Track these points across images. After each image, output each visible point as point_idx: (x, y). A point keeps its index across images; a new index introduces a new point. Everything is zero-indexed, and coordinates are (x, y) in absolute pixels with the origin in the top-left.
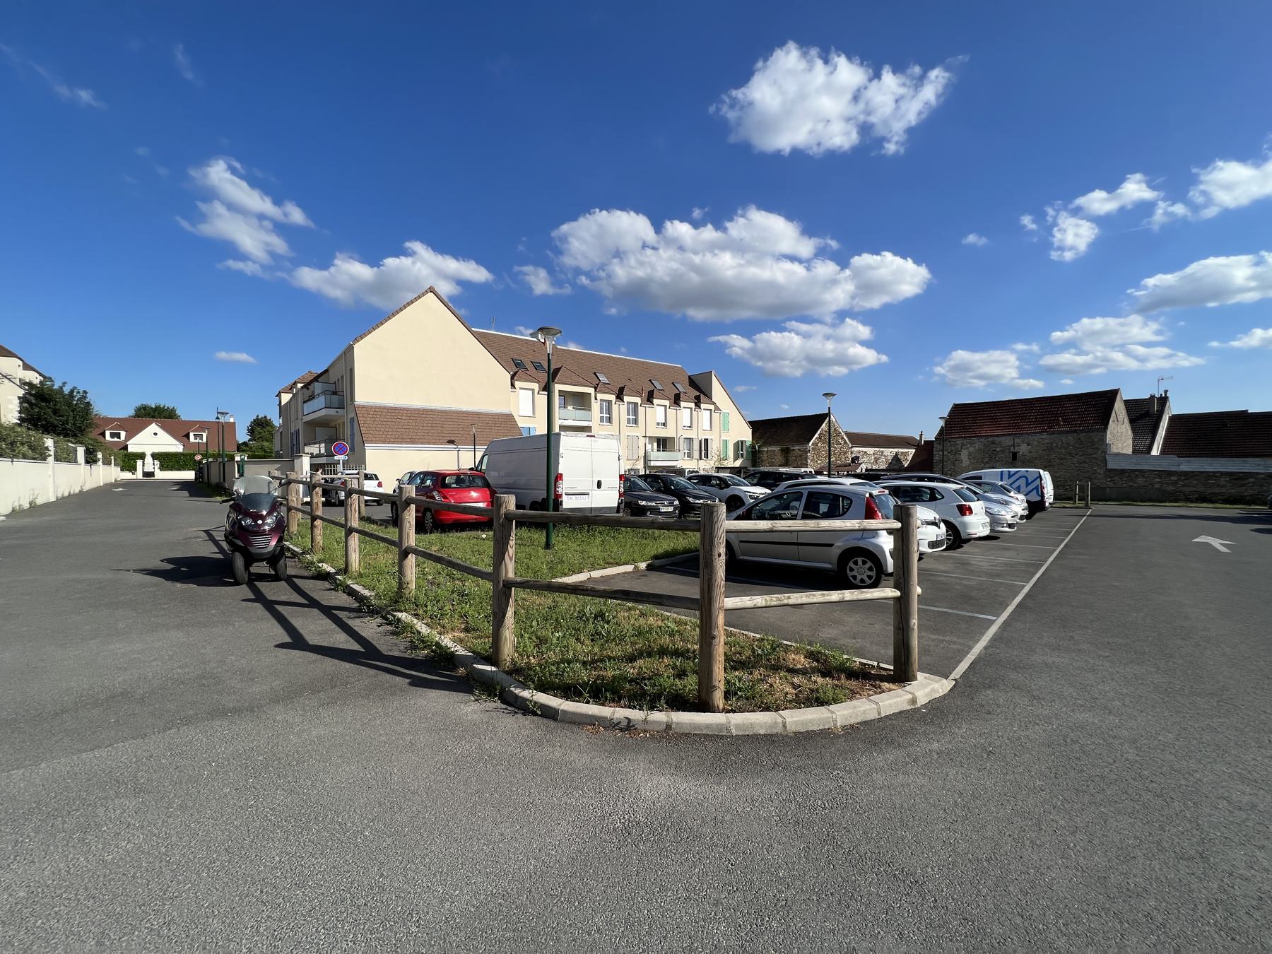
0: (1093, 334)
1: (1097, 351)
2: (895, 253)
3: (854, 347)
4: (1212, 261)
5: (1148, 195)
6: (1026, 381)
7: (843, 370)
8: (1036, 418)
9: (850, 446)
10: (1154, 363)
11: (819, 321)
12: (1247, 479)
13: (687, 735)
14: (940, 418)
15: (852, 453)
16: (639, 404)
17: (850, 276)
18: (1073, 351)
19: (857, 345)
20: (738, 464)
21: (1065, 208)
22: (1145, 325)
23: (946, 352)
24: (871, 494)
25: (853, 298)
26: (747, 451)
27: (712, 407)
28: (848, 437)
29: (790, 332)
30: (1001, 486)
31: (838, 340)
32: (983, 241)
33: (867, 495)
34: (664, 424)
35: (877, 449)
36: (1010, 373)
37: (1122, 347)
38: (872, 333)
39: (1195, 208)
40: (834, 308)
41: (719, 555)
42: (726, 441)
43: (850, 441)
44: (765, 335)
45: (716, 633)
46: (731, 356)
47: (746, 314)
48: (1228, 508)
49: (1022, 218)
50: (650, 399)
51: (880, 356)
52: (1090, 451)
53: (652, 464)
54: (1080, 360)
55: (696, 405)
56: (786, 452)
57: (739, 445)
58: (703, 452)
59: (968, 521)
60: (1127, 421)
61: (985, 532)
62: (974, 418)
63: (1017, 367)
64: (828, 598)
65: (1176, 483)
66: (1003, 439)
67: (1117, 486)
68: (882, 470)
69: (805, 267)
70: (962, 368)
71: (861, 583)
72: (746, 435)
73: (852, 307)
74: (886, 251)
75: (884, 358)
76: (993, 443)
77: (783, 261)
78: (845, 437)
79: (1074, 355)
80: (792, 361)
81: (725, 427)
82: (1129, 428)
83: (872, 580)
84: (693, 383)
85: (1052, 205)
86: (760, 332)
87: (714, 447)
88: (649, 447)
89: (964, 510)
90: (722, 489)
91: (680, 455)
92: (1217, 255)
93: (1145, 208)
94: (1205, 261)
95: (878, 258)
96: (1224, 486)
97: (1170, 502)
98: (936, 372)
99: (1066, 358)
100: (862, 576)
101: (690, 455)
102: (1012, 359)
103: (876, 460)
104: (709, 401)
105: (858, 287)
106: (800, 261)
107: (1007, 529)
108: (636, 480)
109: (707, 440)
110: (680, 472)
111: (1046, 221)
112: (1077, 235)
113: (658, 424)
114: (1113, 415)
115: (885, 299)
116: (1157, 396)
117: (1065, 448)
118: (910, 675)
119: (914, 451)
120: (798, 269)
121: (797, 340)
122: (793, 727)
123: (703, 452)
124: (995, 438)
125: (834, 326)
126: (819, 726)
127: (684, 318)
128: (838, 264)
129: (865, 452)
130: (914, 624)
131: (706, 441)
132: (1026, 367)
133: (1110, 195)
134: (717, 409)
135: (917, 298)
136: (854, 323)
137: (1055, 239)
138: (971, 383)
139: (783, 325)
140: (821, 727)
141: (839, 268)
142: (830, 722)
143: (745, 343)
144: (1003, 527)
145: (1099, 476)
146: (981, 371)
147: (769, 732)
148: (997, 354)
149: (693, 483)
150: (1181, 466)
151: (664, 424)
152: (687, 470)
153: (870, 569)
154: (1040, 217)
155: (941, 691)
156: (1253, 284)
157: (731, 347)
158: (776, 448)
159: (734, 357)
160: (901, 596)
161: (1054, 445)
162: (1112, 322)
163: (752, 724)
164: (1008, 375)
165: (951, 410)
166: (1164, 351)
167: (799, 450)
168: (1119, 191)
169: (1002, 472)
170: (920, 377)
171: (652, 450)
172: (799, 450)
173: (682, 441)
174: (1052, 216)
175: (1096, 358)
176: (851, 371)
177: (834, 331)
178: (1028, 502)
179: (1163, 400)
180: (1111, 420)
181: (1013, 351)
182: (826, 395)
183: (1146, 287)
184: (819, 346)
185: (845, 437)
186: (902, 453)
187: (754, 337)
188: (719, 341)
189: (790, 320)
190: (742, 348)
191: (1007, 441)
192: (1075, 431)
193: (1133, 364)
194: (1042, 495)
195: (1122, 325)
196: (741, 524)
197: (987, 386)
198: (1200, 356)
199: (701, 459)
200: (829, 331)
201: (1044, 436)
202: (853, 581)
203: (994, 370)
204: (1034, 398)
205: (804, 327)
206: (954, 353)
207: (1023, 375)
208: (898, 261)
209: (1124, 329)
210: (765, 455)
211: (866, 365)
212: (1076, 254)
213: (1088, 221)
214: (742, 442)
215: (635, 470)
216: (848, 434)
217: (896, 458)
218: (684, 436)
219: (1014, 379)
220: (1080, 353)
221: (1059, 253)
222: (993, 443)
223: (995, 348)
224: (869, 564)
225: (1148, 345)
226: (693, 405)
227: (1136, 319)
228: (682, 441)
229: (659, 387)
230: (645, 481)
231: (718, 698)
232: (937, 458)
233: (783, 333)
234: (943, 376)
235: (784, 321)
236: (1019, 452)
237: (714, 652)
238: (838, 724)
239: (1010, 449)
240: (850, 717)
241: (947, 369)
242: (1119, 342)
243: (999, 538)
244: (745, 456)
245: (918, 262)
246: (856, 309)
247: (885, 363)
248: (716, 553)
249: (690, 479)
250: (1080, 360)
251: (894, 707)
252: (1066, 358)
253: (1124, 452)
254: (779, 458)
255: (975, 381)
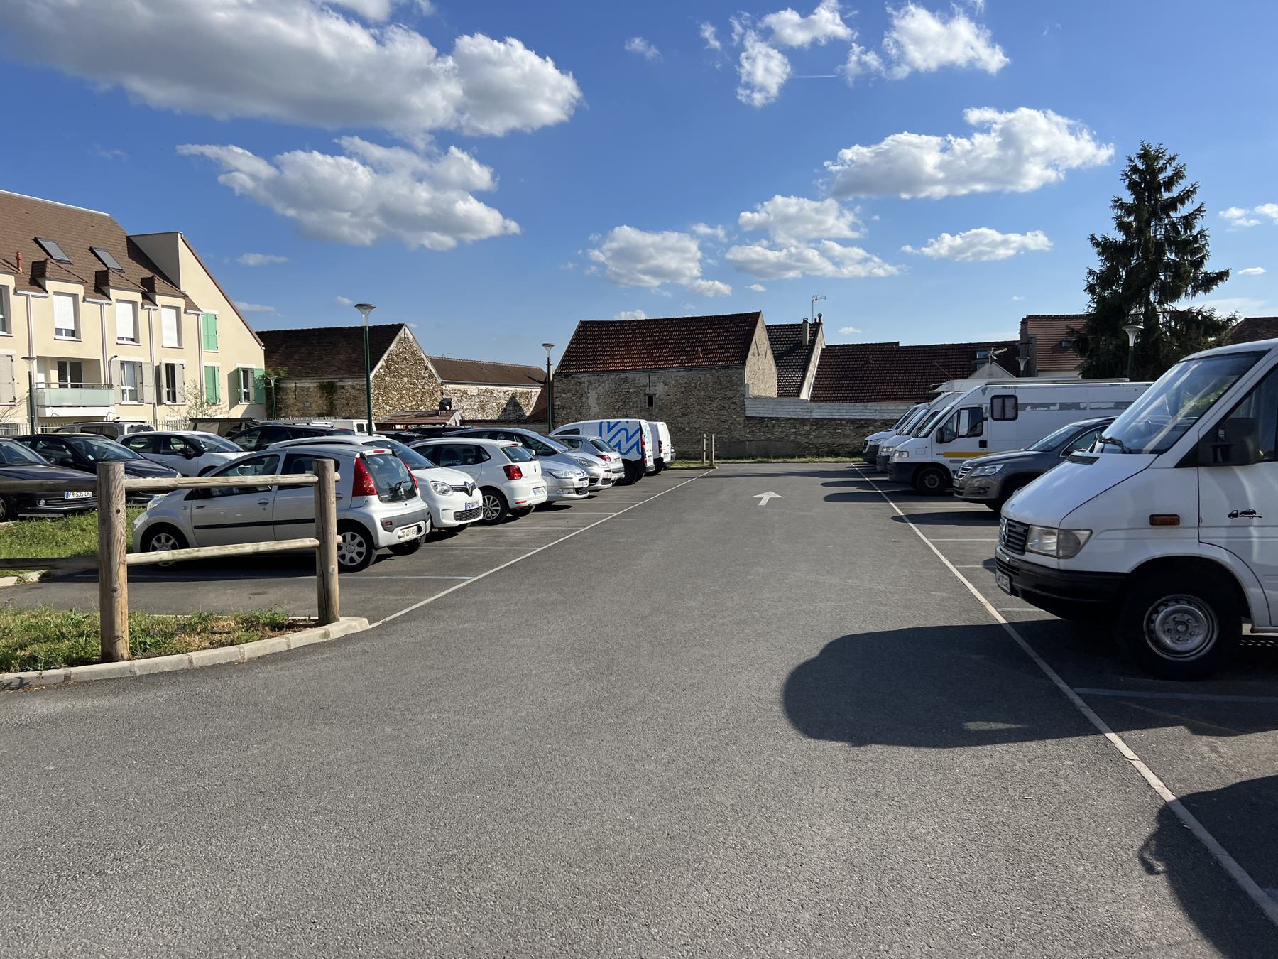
0: (786, 219)
1: (791, 246)
2: (528, 46)
3: (465, 200)
4: (905, 137)
5: (842, 31)
6: (711, 283)
7: (448, 241)
8: (674, 348)
9: (440, 381)
10: (850, 268)
11: (406, 146)
12: (867, 427)
13: (88, 682)
14: (544, 345)
15: (443, 394)
16: (11, 291)
17: (453, 68)
18: (765, 242)
19: (470, 197)
20: (238, 412)
21: (754, 27)
22: (841, 215)
23: (606, 228)
24: (362, 455)
25: (460, 110)
26: (256, 388)
27: (180, 303)
28: (435, 367)
29: (350, 157)
30: (593, 442)
31: (439, 184)
32: (652, 52)
33: (358, 456)
34: (73, 333)
35: (484, 387)
36: (690, 269)
37: (816, 243)
38: (493, 178)
39: (888, 62)
40: (428, 123)
41: (118, 512)
42: (213, 370)
43: (439, 374)
44: (301, 156)
45: (117, 586)
46: (232, 190)
47: (258, 108)
48: (745, 463)
49: (703, 27)
50: (37, 277)
51: (507, 222)
52: (729, 393)
53: (49, 412)
54: (772, 256)
55: (145, 296)
56: (329, 390)
57: (239, 378)
58: (165, 391)
59: (514, 487)
60: (770, 354)
61: (542, 497)
62: (604, 343)
63: (700, 261)
64: (241, 549)
65: (807, 434)
66: (637, 376)
67: (755, 439)
68: (493, 422)
69: (374, 37)
70: (629, 255)
71: (351, 563)
72: (254, 358)
73: (460, 127)
74: (519, 39)
75: (513, 227)
76: (626, 381)
77: (331, 17)
78: (430, 366)
79: (766, 248)
80: (355, 213)
81: (209, 340)
82: (772, 362)
83: (362, 558)
84: (135, 250)
85: (739, 17)
86: (291, 148)
87: (188, 379)
88: (39, 378)
89: (512, 473)
90: (189, 457)
91: (113, 395)
92: (912, 131)
93: (837, 48)
94: (899, 135)
95: (501, 46)
96: (848, 436)
97: (799, 457)
98: (594, 259)
99: (756, 252)
100: (351, 555)
101: (135, 396)
102: (693, 246)
103: (482, 405)
104: (173, 290)
105: (469, 92)
106: (365, 23)
107: (574, 495)
108: (13, 446)
109: (173, 366)
110: (111, 430)
111: (733, 40)
112: (767, 70)
113: (59, 332)
114: (753, 346)
115: (512, 122)
116: (811, 321)
117: (703, 390)
118: (331, 616)
119: (539, 390)
120: (361, 38)
121: (363, 175)
122: (200, 662)
123: (165, 391)
124: (627, 375)
125: (429, 156)
126: (227, 659)
127: (120, 94)
128: (433, 43)
129: (465, 392)
130: (334, 569)
131: (170, 368)
132: (710, 261)
133: (804, 20)
134: (191, 306)
135: (560, 127)
136: (464, 157)
137: (742, 71)
138: (642, 281)
139: (336, 141)
140: (228, 660)
141: (433, 51)
142: (237, 655)
143: (262, 168)
144: (569, 493)
145: (739, 427)
146: (653, 262)
147: (175, 669)
148: (672, 238)
149: (131, 448)
150: (813, 413)
151: (73, 333)
152: (126, 426)
153: (360, 545)
154: (724, 32)
155: (359, 627)
156: (941, 175)
157: (230, 172)
158: (310, 384)
159: (237, 191)
160: (320, 545)
161: (693, 384)
162: (808, 204)
163: (156, 664)
164: (688, 273)
165: (577, 331)
166: (858, 252)
167: (353, 387)
168: (813, 17)
169: (601, 423)
170: (570, 265)
171: (48, 385)
172: (353, 387)
173: (116, 368)
174: (738, 35)
175: (790, 255)
176: (461, 243)
177: (431, 166)
178: (624, 461)
179: (816, 326)
180: (750, 354)
181: (694, 235)
182: (359, 306)
183: (843, 163)
184: (403, 190)
185: (430, 366)
186: (522, 393)
187: (279, 157)
188: (202, 154)
189: (351, 133)
190: (254, 177)
191: (641, 379)
192: (713, 368)
193: (829, 268)
194: (643, 453)
195: (817, 211)
196: (142, 482)
197: (662, 286)
198: (894, 264)
199: (160, 402)
200: (423, 166)
201: (682, 373)
202: (355, 564)
203: (670, 262)
204: (673, 319)
205: (377, 152)
206: (617, 230)
207: (707, 274)
208: (532, 58)
209: (819, 217)
210: (291, 396)
211: (484, 236)
212: (767, 98)
213: (779, 52)
214: (245, 371)
215: (8, 425)
216: (435, 362)
217: (513, 403)
218: (121, 358)
219: (697, 278)
220: (771, 248)
221: (748, 92)
222: (626, 381)
223: (672, 227)
224: (359, 538)
225: (844, 242)
226: (137, 297)
227: (831, 203)
228: (116, 368)
229: (57, 253)
230: (33, 446)
231: (123, 647)
232: (558, 403)
233: (337, 157)
234: (602, 266)
235: (339, 134)
236: (655, 395)
237: (116, 604)
238: (246, 657)
239: (645, 390)
240: (258, 650)
241: (609, 254)
242: (815, 235)
243: (570, 507)
244: (252, 397)
245: (560, 66)
246: (467, 133)
247: (515, 234)
248: (114, 510)
249: (126, 442)
250: (772, 256)
251: (304, 641)
252: (756, 252)
253: (768, 395)
254: (318, 402)
255: (646, 278)
